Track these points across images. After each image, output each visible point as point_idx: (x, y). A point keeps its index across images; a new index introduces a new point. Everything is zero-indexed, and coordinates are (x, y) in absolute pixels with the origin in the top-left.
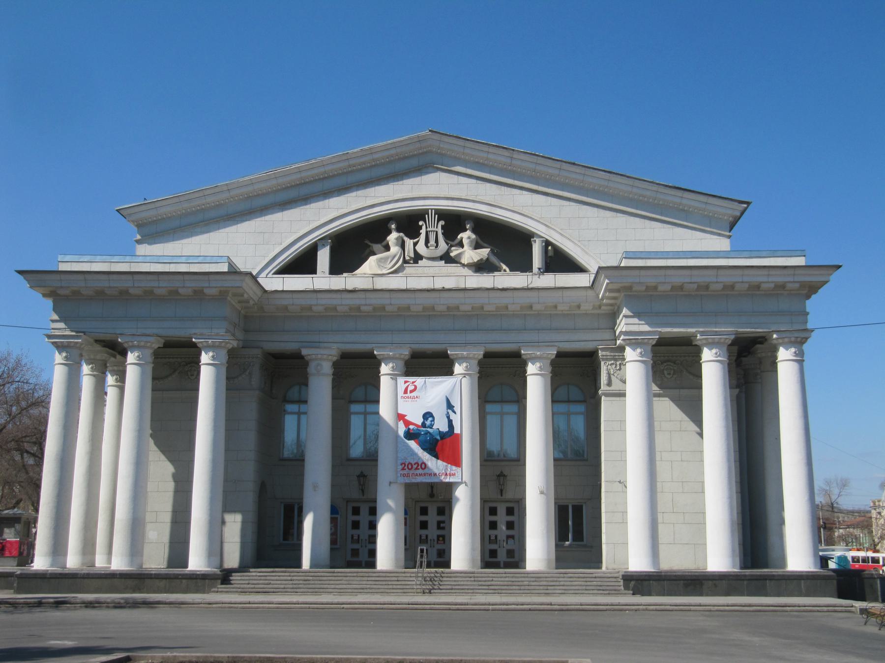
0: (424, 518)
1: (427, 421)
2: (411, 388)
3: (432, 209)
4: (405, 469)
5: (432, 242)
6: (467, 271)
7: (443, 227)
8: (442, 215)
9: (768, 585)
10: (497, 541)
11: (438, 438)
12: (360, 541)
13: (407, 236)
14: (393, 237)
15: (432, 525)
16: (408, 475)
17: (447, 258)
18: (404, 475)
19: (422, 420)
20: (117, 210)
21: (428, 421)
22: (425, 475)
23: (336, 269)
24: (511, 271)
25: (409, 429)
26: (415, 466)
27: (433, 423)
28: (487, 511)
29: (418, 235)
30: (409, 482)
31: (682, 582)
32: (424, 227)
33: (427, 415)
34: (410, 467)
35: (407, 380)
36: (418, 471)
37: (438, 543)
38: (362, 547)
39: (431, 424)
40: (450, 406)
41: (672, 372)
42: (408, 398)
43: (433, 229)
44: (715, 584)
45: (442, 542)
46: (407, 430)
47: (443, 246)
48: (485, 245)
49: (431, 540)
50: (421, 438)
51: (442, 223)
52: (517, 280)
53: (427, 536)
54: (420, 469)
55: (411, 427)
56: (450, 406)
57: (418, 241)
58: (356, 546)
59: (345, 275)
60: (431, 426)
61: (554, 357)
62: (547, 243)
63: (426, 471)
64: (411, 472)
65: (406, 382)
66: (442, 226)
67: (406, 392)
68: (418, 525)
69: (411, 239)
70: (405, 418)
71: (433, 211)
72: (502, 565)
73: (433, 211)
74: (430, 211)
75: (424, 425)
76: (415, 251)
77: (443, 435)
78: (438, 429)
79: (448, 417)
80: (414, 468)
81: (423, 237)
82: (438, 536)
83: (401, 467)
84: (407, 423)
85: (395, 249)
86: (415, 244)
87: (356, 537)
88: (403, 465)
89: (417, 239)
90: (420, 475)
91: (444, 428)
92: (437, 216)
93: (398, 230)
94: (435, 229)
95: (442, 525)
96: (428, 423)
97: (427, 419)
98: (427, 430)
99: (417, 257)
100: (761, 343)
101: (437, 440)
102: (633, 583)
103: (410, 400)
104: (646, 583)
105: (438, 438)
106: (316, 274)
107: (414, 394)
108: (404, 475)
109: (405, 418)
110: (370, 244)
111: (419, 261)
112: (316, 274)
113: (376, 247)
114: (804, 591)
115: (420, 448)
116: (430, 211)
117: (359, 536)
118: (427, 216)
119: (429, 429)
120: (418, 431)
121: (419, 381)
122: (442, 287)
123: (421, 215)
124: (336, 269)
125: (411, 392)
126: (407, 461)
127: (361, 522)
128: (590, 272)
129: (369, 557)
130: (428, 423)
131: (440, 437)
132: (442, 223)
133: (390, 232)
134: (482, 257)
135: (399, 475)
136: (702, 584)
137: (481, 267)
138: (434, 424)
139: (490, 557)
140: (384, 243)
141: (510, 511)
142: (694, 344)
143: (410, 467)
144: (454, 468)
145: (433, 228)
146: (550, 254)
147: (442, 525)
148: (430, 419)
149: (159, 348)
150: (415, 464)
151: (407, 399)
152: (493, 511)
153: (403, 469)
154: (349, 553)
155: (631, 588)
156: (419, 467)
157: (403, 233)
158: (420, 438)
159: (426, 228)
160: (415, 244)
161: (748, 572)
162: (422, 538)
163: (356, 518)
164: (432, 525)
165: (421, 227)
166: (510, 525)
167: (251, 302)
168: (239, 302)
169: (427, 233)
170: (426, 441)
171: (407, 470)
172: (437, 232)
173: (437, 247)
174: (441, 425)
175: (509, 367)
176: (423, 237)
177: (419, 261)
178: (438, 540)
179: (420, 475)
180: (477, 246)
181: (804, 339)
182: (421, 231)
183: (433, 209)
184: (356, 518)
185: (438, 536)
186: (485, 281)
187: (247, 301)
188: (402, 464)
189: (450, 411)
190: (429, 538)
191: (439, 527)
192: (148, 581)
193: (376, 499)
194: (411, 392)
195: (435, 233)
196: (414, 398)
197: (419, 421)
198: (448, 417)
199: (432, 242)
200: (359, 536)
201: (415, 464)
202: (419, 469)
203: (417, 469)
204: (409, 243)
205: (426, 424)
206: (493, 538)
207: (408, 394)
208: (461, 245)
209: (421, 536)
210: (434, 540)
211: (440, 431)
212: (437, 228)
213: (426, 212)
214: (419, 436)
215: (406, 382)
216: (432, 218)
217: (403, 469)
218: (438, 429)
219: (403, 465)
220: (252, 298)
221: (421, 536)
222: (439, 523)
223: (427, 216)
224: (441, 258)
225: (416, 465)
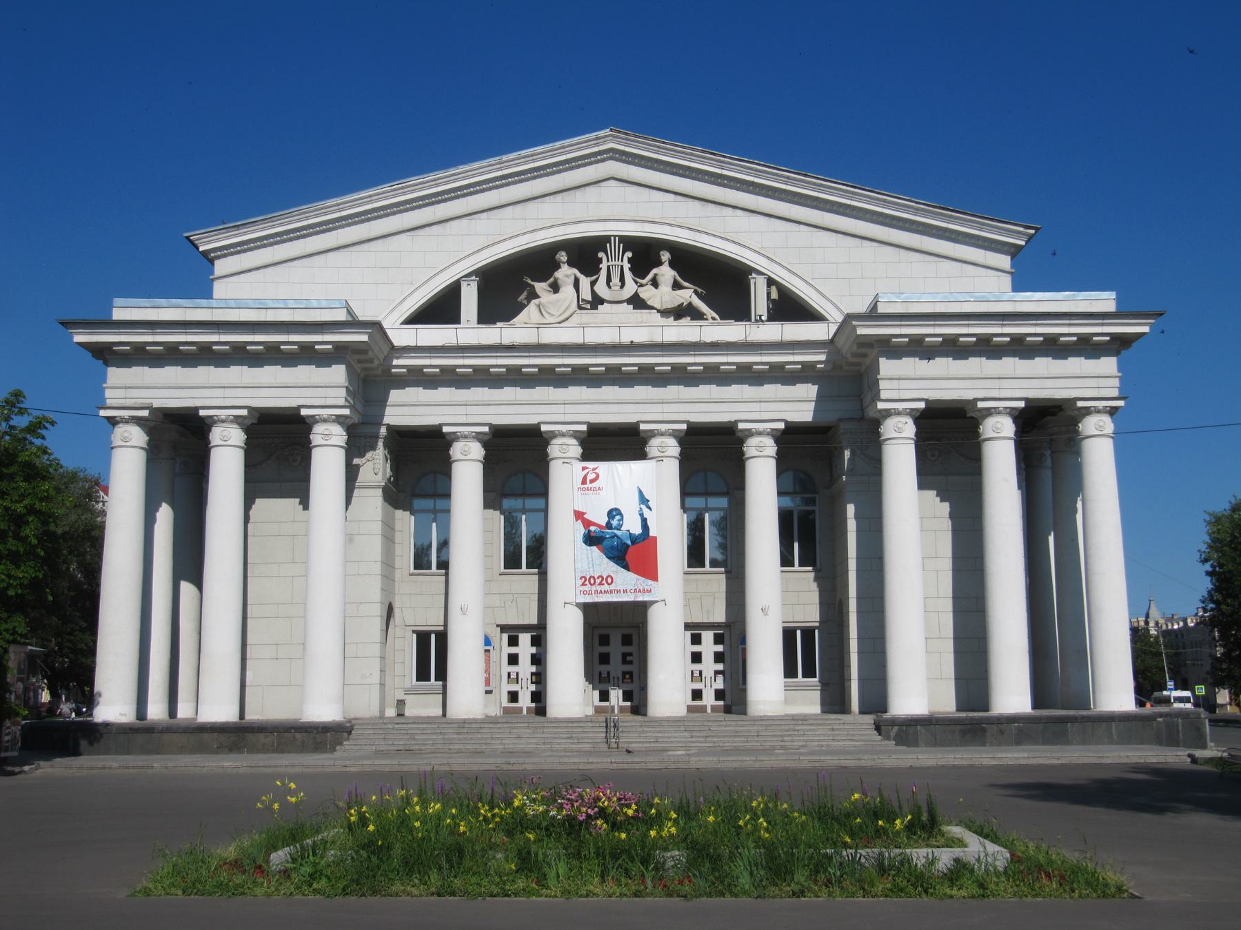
0: (604, 649)
1: (613, 520)
2: (591, 476)
3: (615, 236)
4: (586, 585)
5: (616, 280)
6: (655, 317)
7: (630, 260)
8: (629, 243)
9: (1069, 730)
10: (609, 679)
11: (629, 542)
12: (611, 678)
13: (582, 272)
14: (566, 273)
15: (616, 658)
16: (590, 593)
17: (637, 302)
18: (585, 593)
19: (606, 519)
20: (186, 237)
21: (615, 520)
22: (611, 592)
23: (487, 316)
24: (721, 319)
25: (589, 531)
26: (598, 581)
27: (621, 522)
28: (596, 640)
29: (597, 271)
30: (591, 601)
31: (959, 727)
32: (604, 259)
33: (613, 513)
34: (592, 581)
35: (585, 466)
36: (603, 586)
37: (623, 682)
38: (522, 688)
39: (619, 525)
40: (644, 500)
41: (937, 453)
42: (588, 489)
43: (617, 263)
44: (1001, 731)
45: (630, 681)
46: (587, 532)
47: (631, 288)
48: (686, 284)
49: (614, 678)
50: (606, 543)
51: (629, 254)
52: (733, 331)
53: (608, 673)
54: (606, 584)
55: (593, 528)
56: (644, 500)
57: (597, 279)
58: (514, 688)
59: (500, 324)
60: (619, 528)
61: (683, 434)
62: (771, 282)
63: (612, 587)
64: (594, 588)
65: (584, 469)
66: (629, 258)
67: (584, 482)
68: (505, 659)
69: (587, 276)
70: (585, 516)
71: (617, 238)
72: (709, 710)
73: (617, 238)
74: (612, 238)
75: (609, 525)
76: (593, 293)
77: (634, 539)
78: (629, 531)
79: (641, 515)
80: (597, 584)
81: (603, 273)
82: (624, 673)
83: (581, 582)
84: (587, 524)
85: (568, 291)
86: (593, 283)
87: (513, 676)
88: (583, 579)
89: (596, 276)
90: (606, 592)
91: (637, 530)
92: (621, 245)
93: (571, 263)
94: (620, 263)
95: (629, 658)
96: (615, 523)
97: (613, 518)
98: (613, 533)
99: (597, 301)
100: (1054, 414)
101: (628, 546)
102: (896, 729)
103: (590, 492)
104: (912, 729)
105: (629, 542)
106: (459, 323)
107: (594, 485)
108: (585, 593)
109: (585, 516)
110: (532, 283)
111: (599, 306)
112: (459, 323)
113: (540, 287)
114: (1115, 737)
115: (604, 556)
116: (612, 238)
117: (517, 674)
118: (608, 245)
119: (616, 531)
120: (601, 534)
121: (603, 467)
122: (630, 340)
123: (600, 243)
124: (487, 316)
125: (592, 481)
126: (588, 573)
127: (510, 652)
128: (828, 320)
129: (601, 700)
130: (615, 523)
131: (632, 542)
132: (629, 254)
133: (557, 266)
134: (682, 301)
135: (578, 592)
136: (984, 731)
137: (681, 312)
138: (622, 525)
139: (601, 700)
140: (552, 280)
141: (627, 640)
142: (968, 416)
143: (592, 581)
144: (650, 582)
145: (616, 262)
146: (774, 295)
147: (629, 658)
148: (618, 517)
149: (253, 424)
150: (598, 578)
151: (586, 492)
152: (605, 640)
153: (583, 584)
154: (505, 697)
155: (892, 738)
156: (604, 582)
157: (576, 268)
158: (604, 543)
159: (608, 261)
160: (593, 283)
161: (963, 715)
162: (603, 676)
163: (513, 650)
164: (616, 658)
165: (600, 261)
166: (625, 658)
167: (376, 362)
168: (359, 361)
169: (608, 267)
170: (612, 547)
171: (589, 585)
172: (622, 267)
173: (622, 286)
174: (632, 526)
175: (696, 448)
176: (603, 273)
177: (599, 306)
178: (624, 677)
179: (606, 592)
180: (676, 286)
181: (1114, 410)
182: (601, 266)
183: (617, 236)
184: (513, 650)
185: (624, 673)
186: (685, 331)
187: (371, 361)
188: (581, 579)
189: (643, 507)
190: (612, 676)
191: (625, 662)
192: (250, 736)
193: (546, 624)
194: (592, 481)
195: (620, 267)
196: (595, 489)
197: (603, 521)
198: (641, 515)
199: (616, 280)
200: (517, 674)
201: (598, 578)
202: (604, 584)
203: (601, 584)
204: (585, 282)
205: (612, 524)
206: (513, 676)
207: (588, 485)
208: (655, 283)
209: (600, 673)
210: (618, 678)
211: (630, 534)
212: (622, 261)
213: (607, 239)
214: (604, 541)
215: (584, 469)
216: (614, 247)
217: (583, 584)
218: (629, 531)
219: (583, 579)
220: (377, 356)
221: (600, 673)
222: (625, 655)
223: (608, 245)
224: (629, 301)
225: (600, 579)
